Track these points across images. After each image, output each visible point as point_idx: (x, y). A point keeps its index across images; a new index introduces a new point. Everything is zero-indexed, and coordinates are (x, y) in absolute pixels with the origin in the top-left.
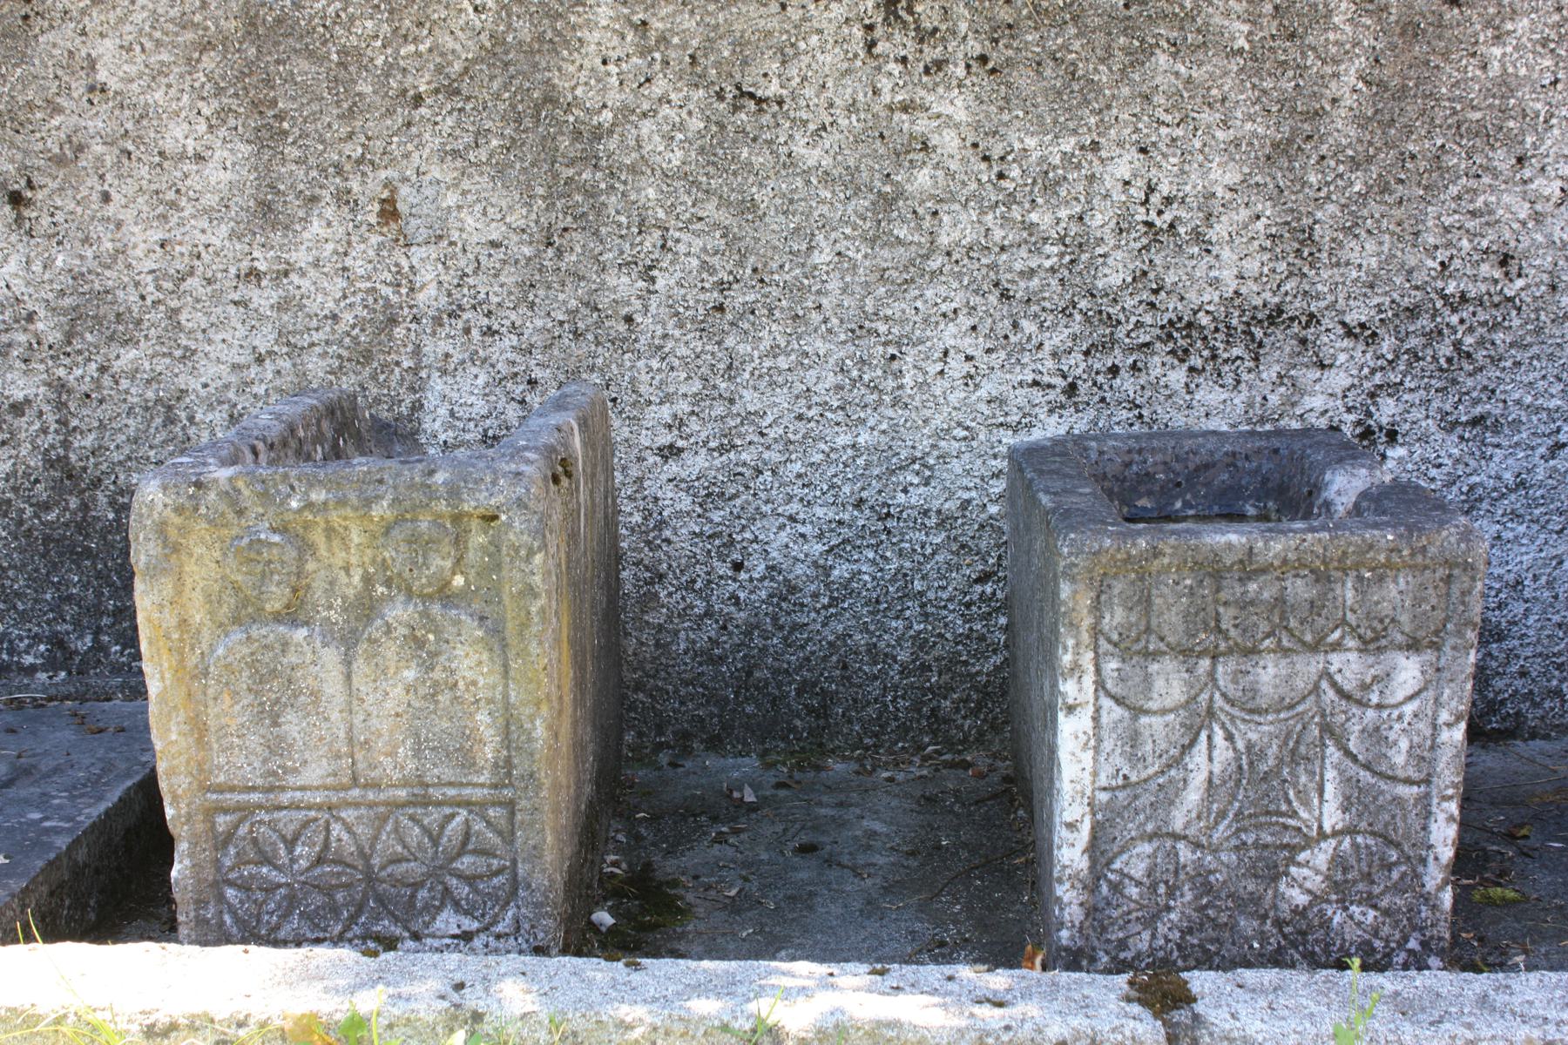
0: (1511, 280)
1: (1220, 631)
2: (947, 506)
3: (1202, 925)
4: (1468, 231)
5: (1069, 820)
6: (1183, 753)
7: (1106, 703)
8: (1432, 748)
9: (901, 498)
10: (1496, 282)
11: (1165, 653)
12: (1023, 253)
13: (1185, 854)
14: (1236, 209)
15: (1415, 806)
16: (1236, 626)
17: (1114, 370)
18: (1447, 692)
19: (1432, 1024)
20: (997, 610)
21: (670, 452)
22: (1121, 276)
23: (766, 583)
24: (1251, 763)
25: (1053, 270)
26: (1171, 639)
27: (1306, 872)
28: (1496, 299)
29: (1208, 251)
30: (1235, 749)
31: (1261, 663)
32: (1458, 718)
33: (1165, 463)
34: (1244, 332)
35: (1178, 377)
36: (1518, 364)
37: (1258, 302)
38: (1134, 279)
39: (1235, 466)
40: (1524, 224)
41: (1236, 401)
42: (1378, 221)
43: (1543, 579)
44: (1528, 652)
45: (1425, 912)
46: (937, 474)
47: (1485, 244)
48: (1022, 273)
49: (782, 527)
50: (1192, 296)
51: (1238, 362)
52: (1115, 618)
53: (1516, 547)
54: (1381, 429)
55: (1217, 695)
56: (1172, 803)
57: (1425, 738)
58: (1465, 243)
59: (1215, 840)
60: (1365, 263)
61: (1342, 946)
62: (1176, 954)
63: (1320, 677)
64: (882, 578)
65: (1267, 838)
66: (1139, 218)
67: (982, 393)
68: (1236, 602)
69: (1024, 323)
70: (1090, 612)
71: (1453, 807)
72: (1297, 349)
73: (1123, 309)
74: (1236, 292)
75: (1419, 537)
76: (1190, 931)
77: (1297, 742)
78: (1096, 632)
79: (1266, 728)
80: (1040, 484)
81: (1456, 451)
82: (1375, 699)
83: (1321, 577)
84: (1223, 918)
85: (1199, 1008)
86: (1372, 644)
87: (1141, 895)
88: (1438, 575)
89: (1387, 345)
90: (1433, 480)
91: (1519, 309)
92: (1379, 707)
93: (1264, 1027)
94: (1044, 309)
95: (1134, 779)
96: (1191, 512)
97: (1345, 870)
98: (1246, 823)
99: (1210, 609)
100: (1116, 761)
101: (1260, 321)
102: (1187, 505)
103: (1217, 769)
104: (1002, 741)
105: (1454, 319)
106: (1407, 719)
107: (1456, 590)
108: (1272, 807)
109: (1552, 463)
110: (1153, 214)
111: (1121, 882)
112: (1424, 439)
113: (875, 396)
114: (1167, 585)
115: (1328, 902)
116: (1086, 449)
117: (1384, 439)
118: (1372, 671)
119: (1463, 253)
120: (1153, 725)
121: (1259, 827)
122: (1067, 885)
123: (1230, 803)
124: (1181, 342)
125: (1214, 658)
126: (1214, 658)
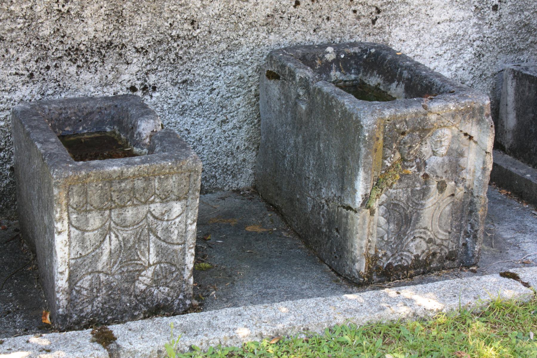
0: (195, 30)
1: (112, 200)
3: (109, 300)
4: (179, 12)
5: (60, 271)
6: (100, 244)
7: (73, 229)
8: (185, 232)
10: (190, 30)
11: (93, 210)
12: (9, 22)
13: (103, 277)
14: (93, 4)
15: (180, 252)
16: (118, 199)
17: (48, 68)
18: (190, 213)
19: (195, 336)
20: (6, 162)
22: (49, 31)
24: (125, 244)
25: (21, 29)
26: (95, 205)
27: (144, 278)
28: (190, 37)
29: (83, 21)
30: (119, 240)
31: (127, 210)
32: (194, 222)
33: (75, 113)
34: (98, 52)
35: (73, 69)
36: (198, 60)
37: (103, 40)
38: (54, 32)
39: (101, 112)
40: (199, 9)
41: (96, 78)
42: (146, 8)
43: (209, 137)
45: (185, 286)
47: (185, 16)
48: (8, 31)
50: (77, 38)
51: (96, 63)
52: (75, 200)
53: (199, 126)
54: (150, 86)
55: (112, 223)
56: (97, 261)
57: (183, 229)
58: (178, 16)
59: (113, 271)
60: (142, 24)
61: (157, 301)
62: (100, 311)
63: (147, 213)
65: (131, 269)
66: (55, 8)
68: (118, 190)
69: (11, 50)
70: (65, 199)
71: (193, 251)
72: (118, 58)
73: (50, 44)
74: (94, 37)
75: (179, 163)
76: (105, 303)
77: (140, 235)
78: (68, 205)
79: (129, 232)
80: (34, 136)
81: (177, 93)
82: (166, 218)
83: (147, 179)
84: (117, 297)
85: (119, 342)
86: (165, 200)
87: (88, 293)
88: (186, 175)
89: (151, 55)
90: (169, 104)
91: (198, 40)
92: (168, 220)
93: (141, 346)
94: (18, 45)
95: (83, 254)
96: (86, 131)
97: (158, 276)
98: (124, 264)
99: (109, 193)
100: (77, 249)
101: (104, 47)
102: (84, 128)
103: (113, 247)
104: (11, 212)
105: (175, 45)
106: (177, 224)
107: (192, 179)
108: (132, 258)
109: (211, 95)
110: (61, 7)
111: (80, 290)
112: (166, 89)
114: (93, 187)
115: (152, 287)
116: (44, 109)
117: (151, 90)
118: (165, 209)
119: (178, 20)
120: (89, 235)
121: (128, 265)
122: (61, 293)
123: (118, 258)
124: (73, 56)
125: (110, 210)
126: (110, 210)
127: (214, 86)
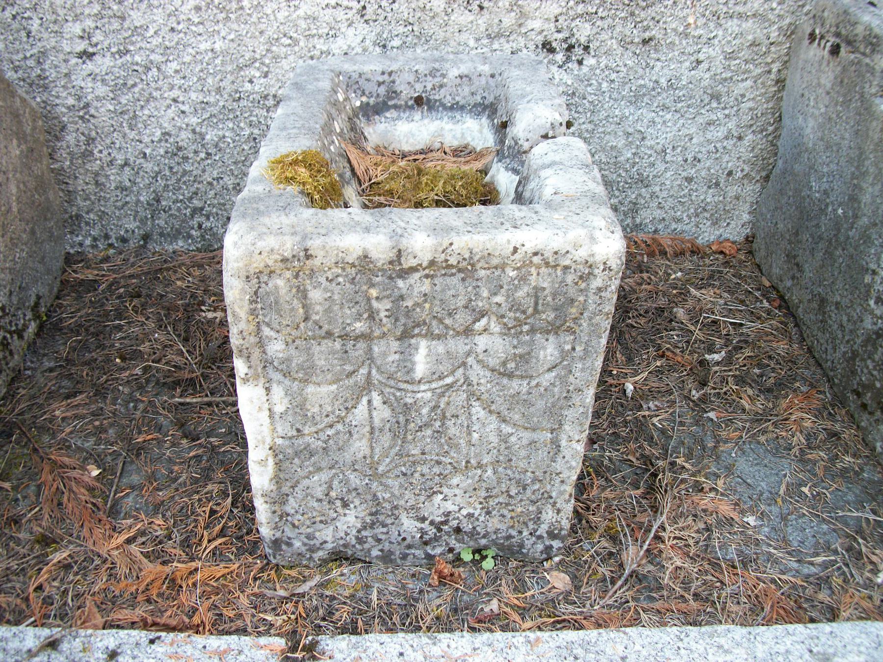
2: (280, 92)
9: (248, 87)
21: (85, 55)
23: (163, 144)
44: (664, 194)
46: (272, 69)
49: (169, 106)
64: (239, 141)
67: (301, 12)
113: (223, 15)
127: (701, 57)
